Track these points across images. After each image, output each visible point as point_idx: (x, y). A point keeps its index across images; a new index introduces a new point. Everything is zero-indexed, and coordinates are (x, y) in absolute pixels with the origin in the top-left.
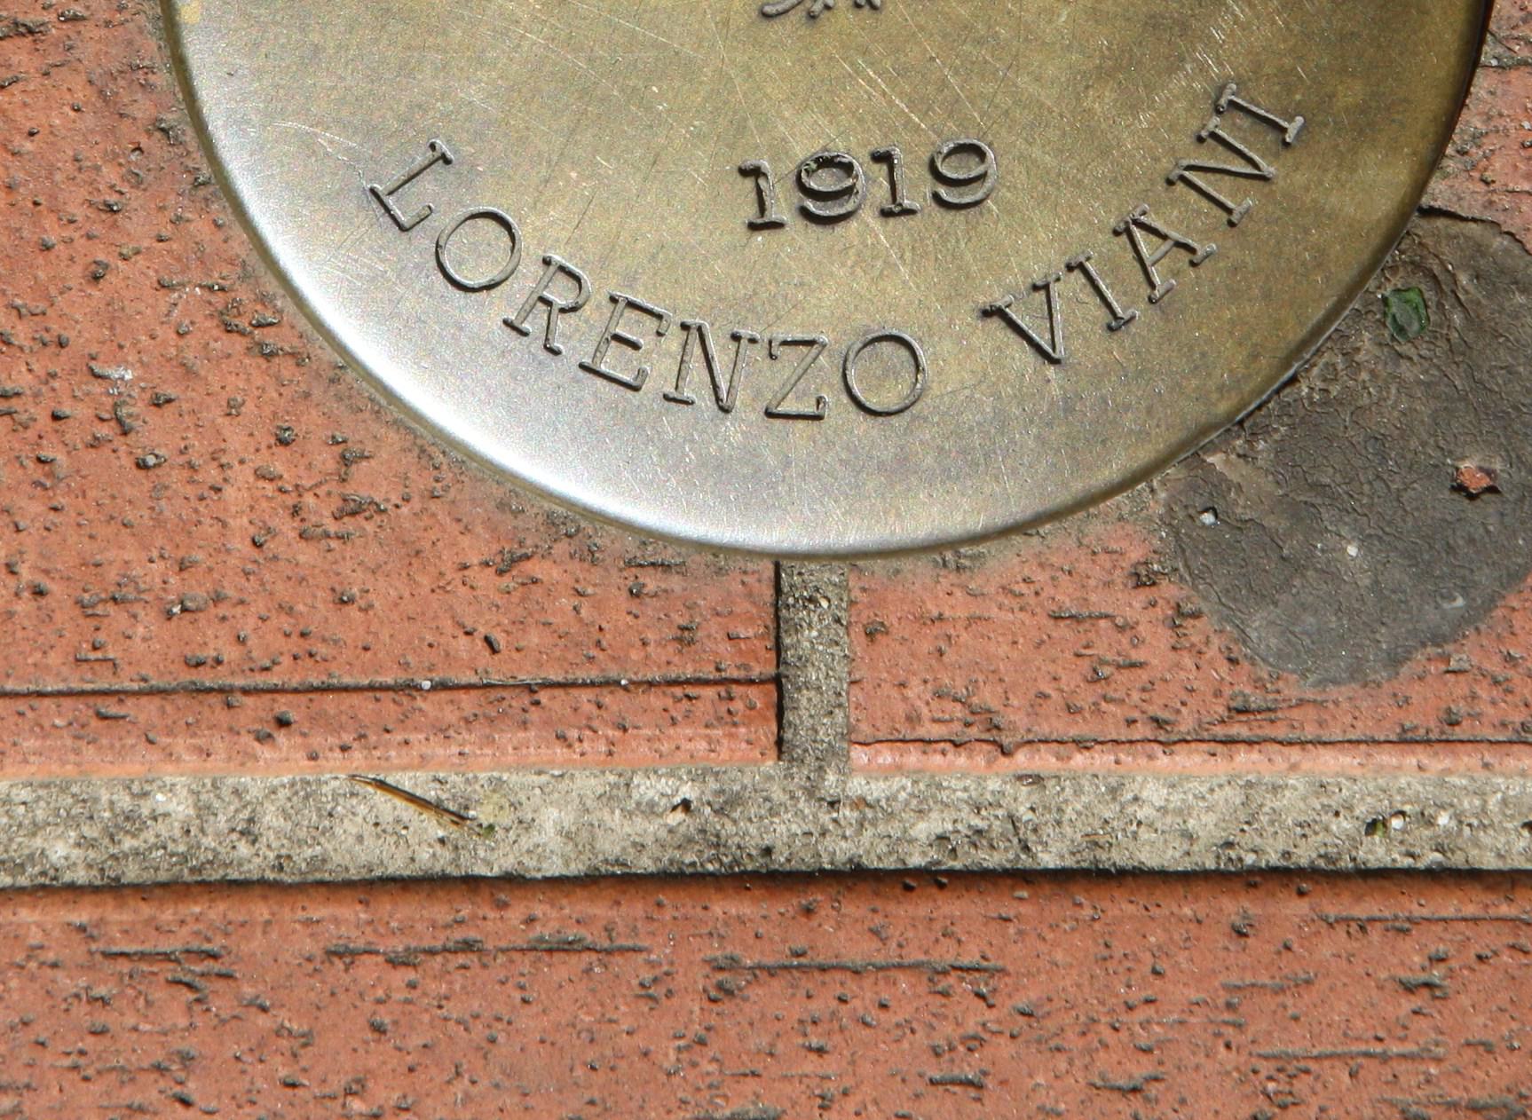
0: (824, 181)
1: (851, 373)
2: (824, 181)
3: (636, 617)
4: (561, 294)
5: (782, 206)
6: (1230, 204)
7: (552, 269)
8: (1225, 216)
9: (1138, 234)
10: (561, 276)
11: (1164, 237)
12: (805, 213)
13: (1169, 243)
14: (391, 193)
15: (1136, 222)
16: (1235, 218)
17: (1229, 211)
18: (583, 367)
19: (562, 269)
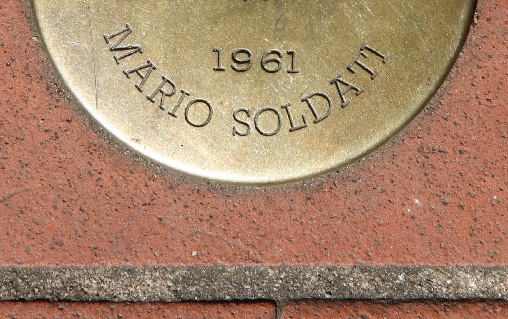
0: (241, 57)
1: (258, 124)
2: (241, 57)
3: (469, 193)
4: (167, 89)
5: (226, 63)
6: (384, 56)
7: (184, 94)
8: (370, 76)
9: (338, 83)
10: (167, 83)
11: (347, 85)
12: (234, 69)
13: (349, 87)
14: (120, 59)
15: (339, 81)
16: (385, 60)
17: (383, 58)
18: (136, 86)
19: (168, 81)
